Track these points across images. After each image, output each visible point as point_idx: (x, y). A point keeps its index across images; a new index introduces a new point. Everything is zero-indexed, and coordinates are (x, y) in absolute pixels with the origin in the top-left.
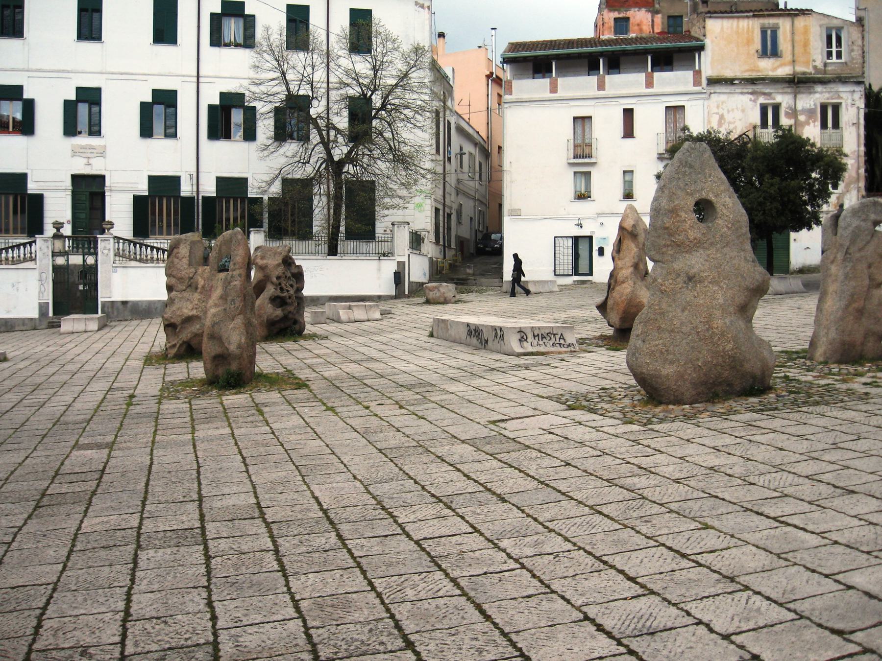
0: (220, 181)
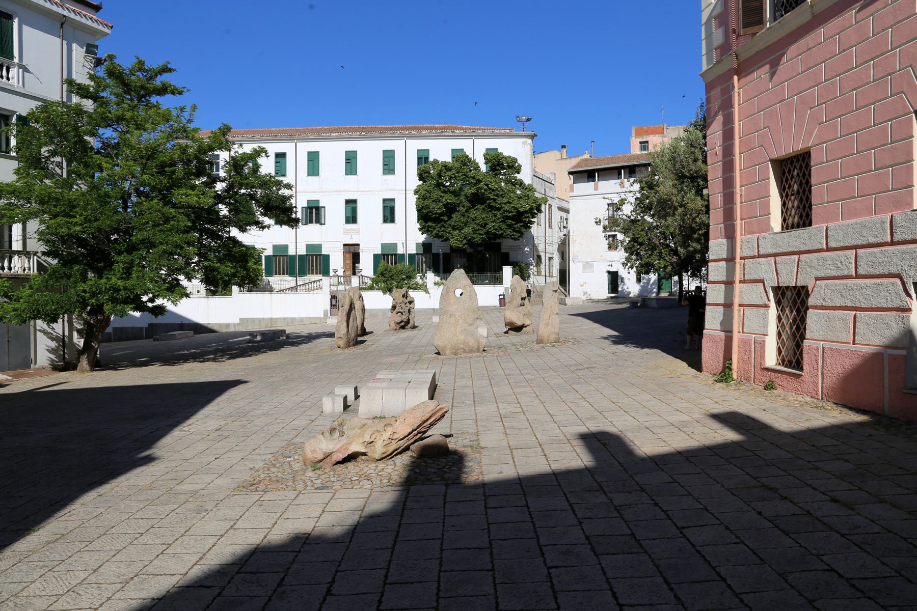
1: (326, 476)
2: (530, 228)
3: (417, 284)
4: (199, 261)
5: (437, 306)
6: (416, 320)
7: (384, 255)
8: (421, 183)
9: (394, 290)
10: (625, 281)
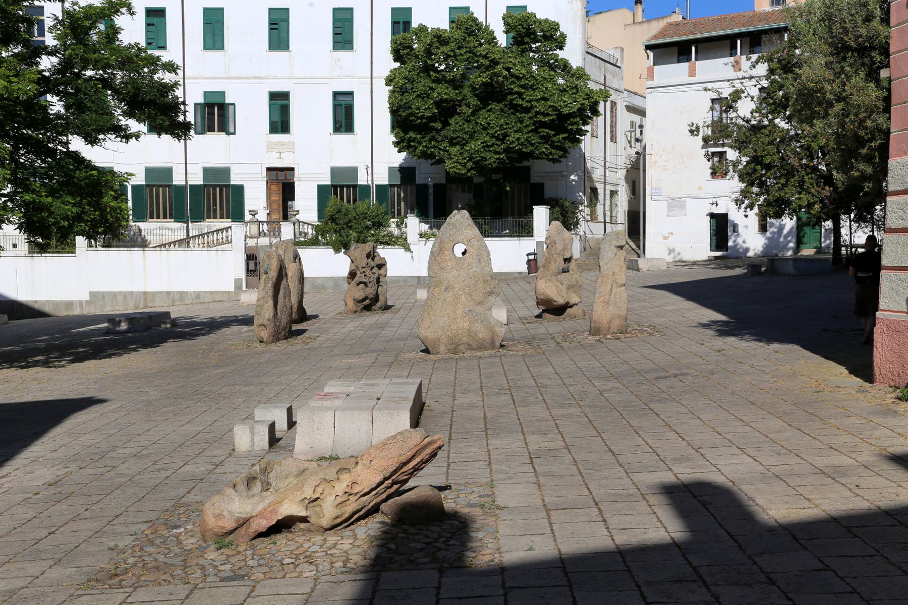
0: (206, 171)
1: (240, 557)
2: (579, 141)
3: (391, 235)
4: (15, 193)
5: (424, 272)
6: (390, 296)
7: (335, 187)
8: (398, 64)
9: (353, 246)
10: (741, 229)
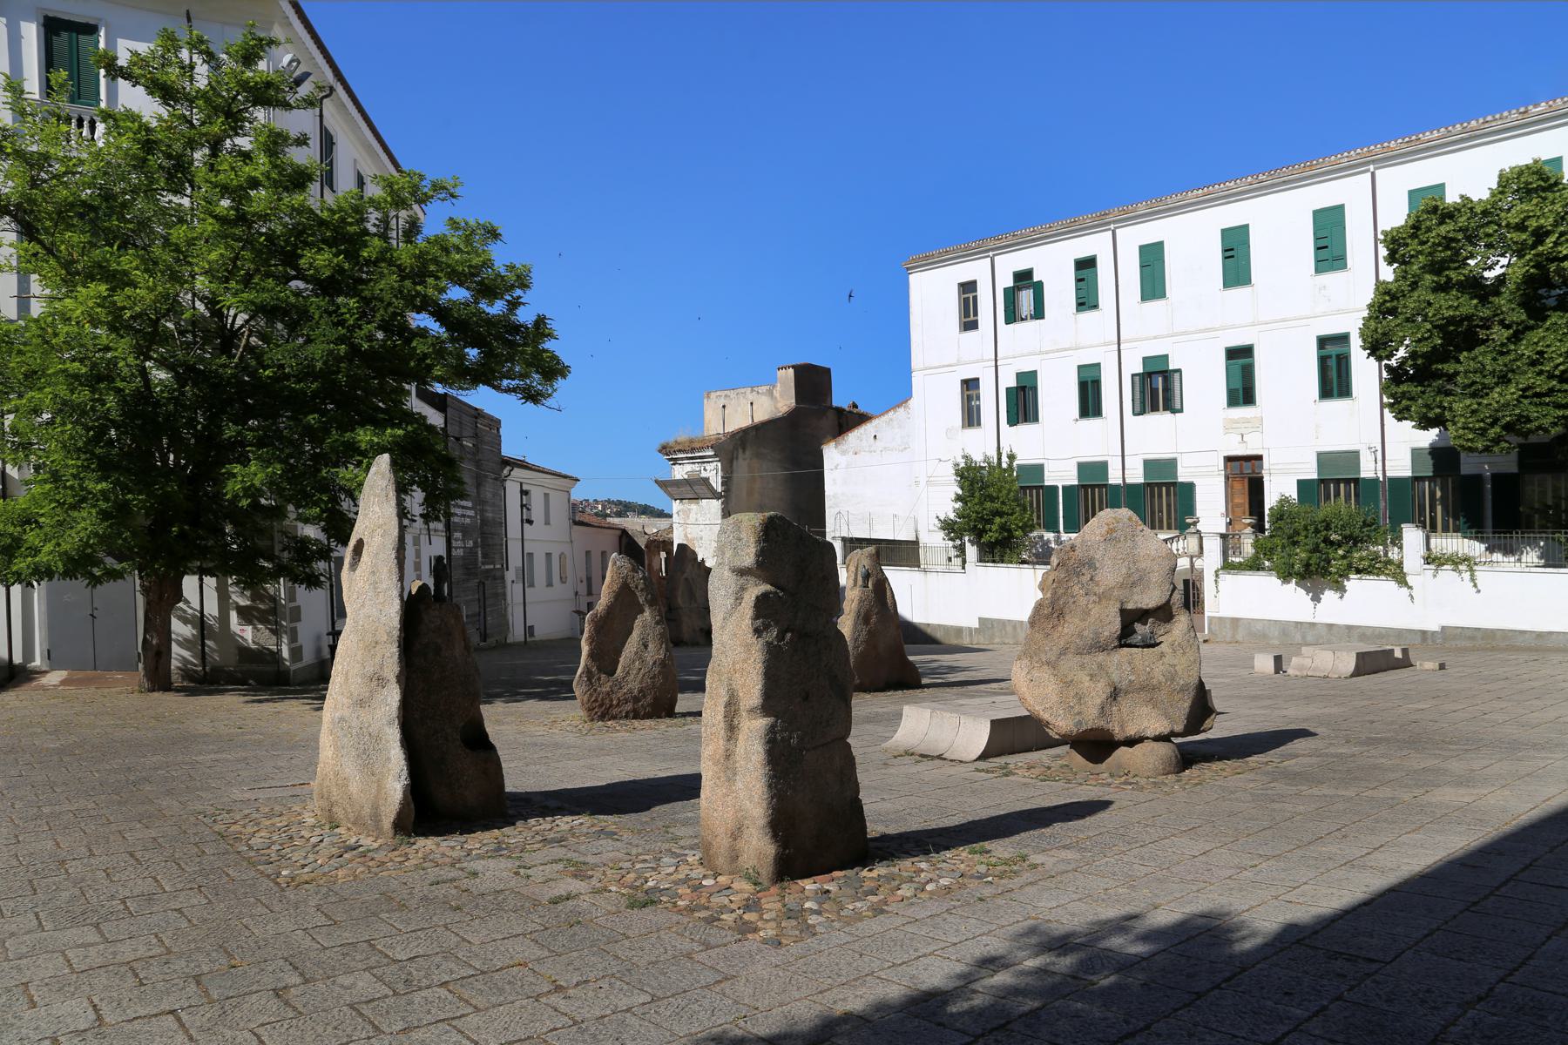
7: (1321, 481)
